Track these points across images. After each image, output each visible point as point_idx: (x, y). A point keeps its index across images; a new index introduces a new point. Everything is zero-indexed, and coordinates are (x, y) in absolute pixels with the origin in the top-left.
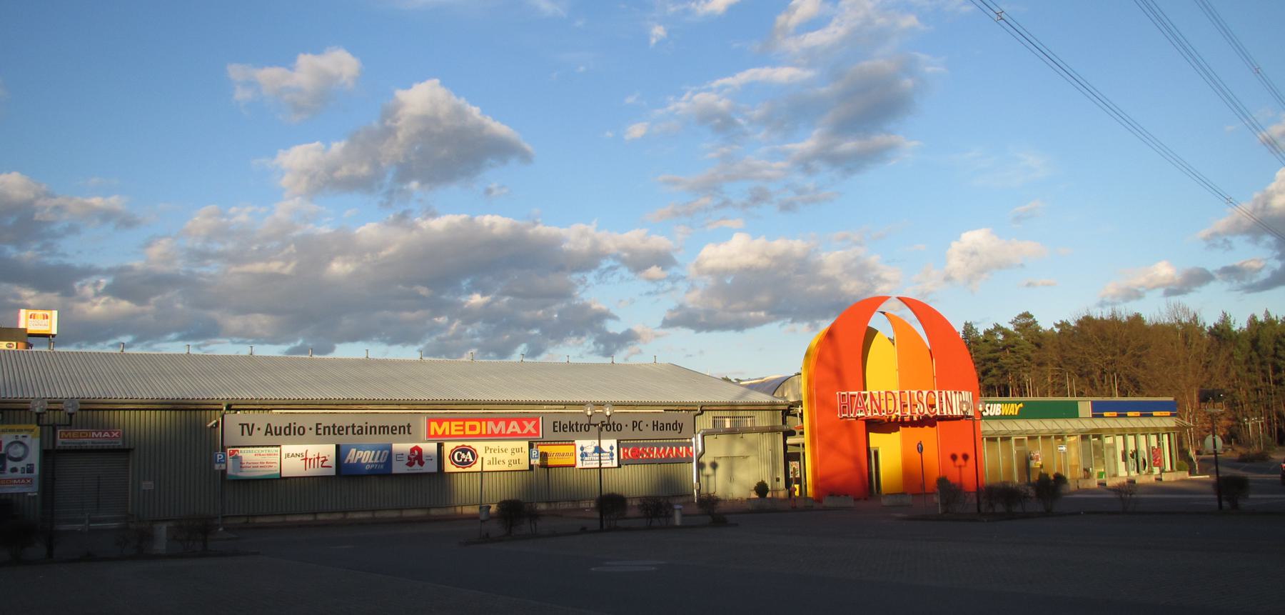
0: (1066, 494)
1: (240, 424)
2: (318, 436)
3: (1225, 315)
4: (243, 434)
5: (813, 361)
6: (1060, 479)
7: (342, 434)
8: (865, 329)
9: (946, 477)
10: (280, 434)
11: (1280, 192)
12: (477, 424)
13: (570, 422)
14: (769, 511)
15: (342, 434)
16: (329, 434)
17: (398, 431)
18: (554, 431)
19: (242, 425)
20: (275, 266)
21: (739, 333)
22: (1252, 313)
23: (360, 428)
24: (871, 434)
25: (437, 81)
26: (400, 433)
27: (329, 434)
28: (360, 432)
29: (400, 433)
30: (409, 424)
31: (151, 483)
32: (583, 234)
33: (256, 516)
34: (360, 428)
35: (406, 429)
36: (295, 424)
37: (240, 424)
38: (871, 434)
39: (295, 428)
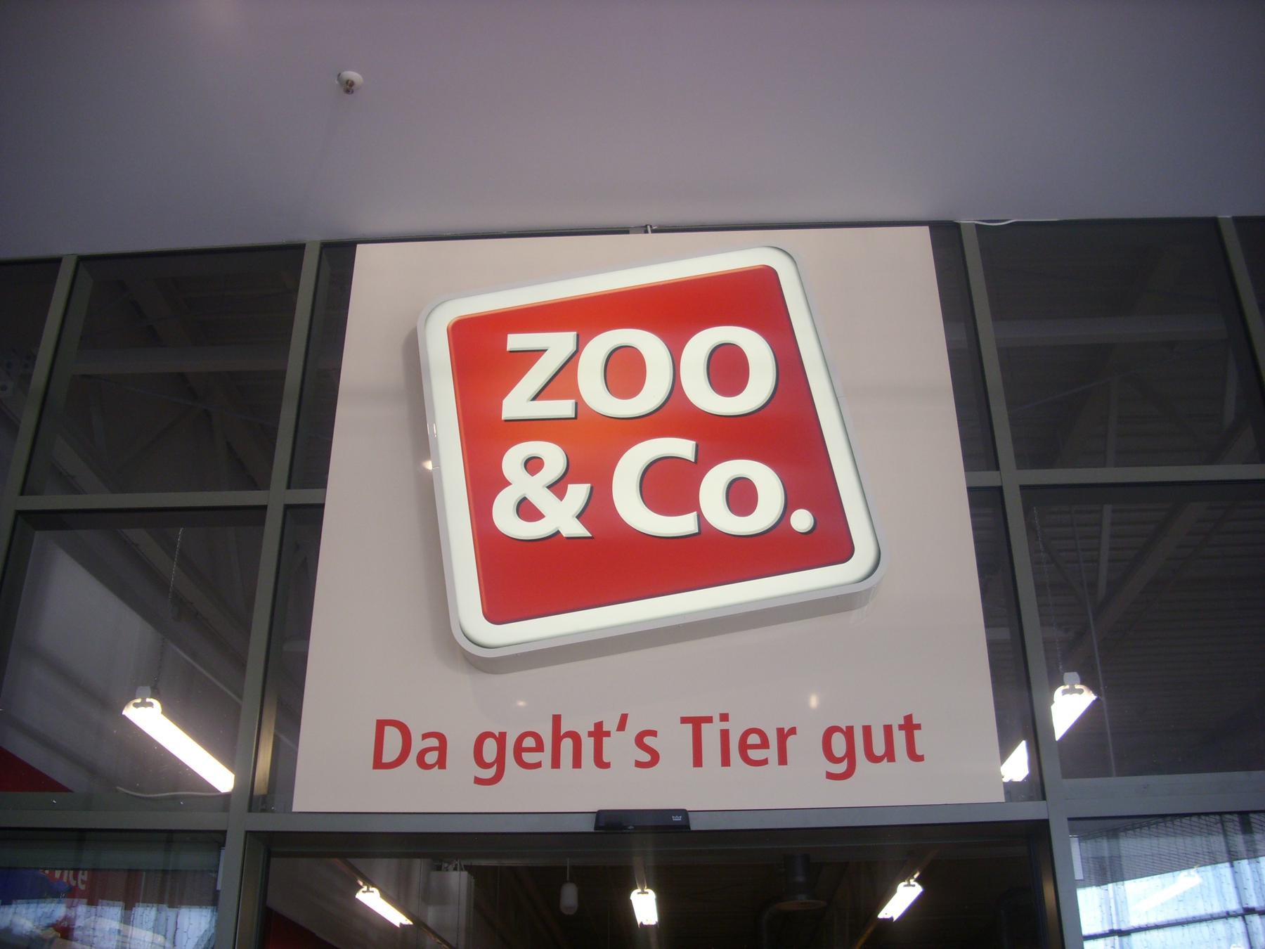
0: (132, 929)
1: (684, 720)
2: (281, 509)
3: (541, 762)
4: (698, 762)
5: (30, 901)
6: (169, 907)
7: (764, 762)
8: (1002, 785)
9: (558, 533)
10: (890, 755)
11: (1219, 947)
12: (649, 345)
13: (557, 720)
14: (1202, 814)
15: (764, 762)
16: (577, 763)
17: (546, 757)
18: (378, 764)
19: (697, 723)
20: (1059, 656)
21: (878, 764)
22: (523, 492)
23: (434, 742)
24: (294, 809)
25: (895, 919)
26: (556, 763)
27: (577, 763)
28: (431, 758)
29: (556, 763)
30: (908, 718)
31: (57, 871)
32: (1251, 896)
33: (166, 928)
34: (434, 742)
35: (588, 745)
36: (724, 717)
37: (684, 720)
38: (294, 809)
39: (725, 735)
